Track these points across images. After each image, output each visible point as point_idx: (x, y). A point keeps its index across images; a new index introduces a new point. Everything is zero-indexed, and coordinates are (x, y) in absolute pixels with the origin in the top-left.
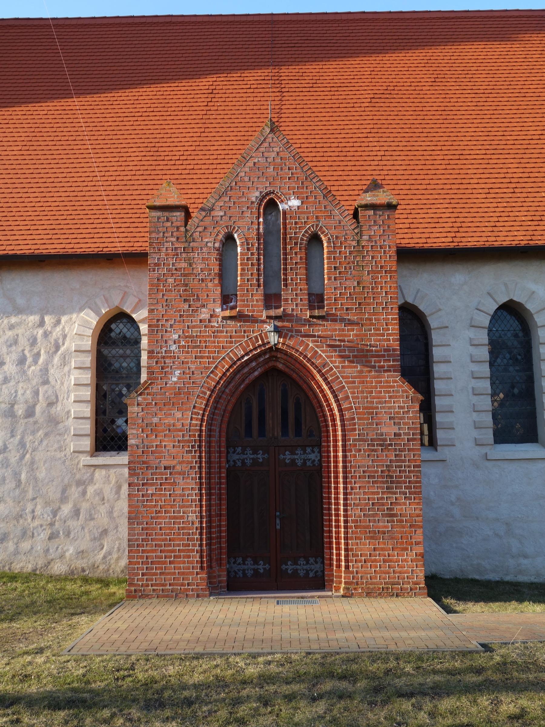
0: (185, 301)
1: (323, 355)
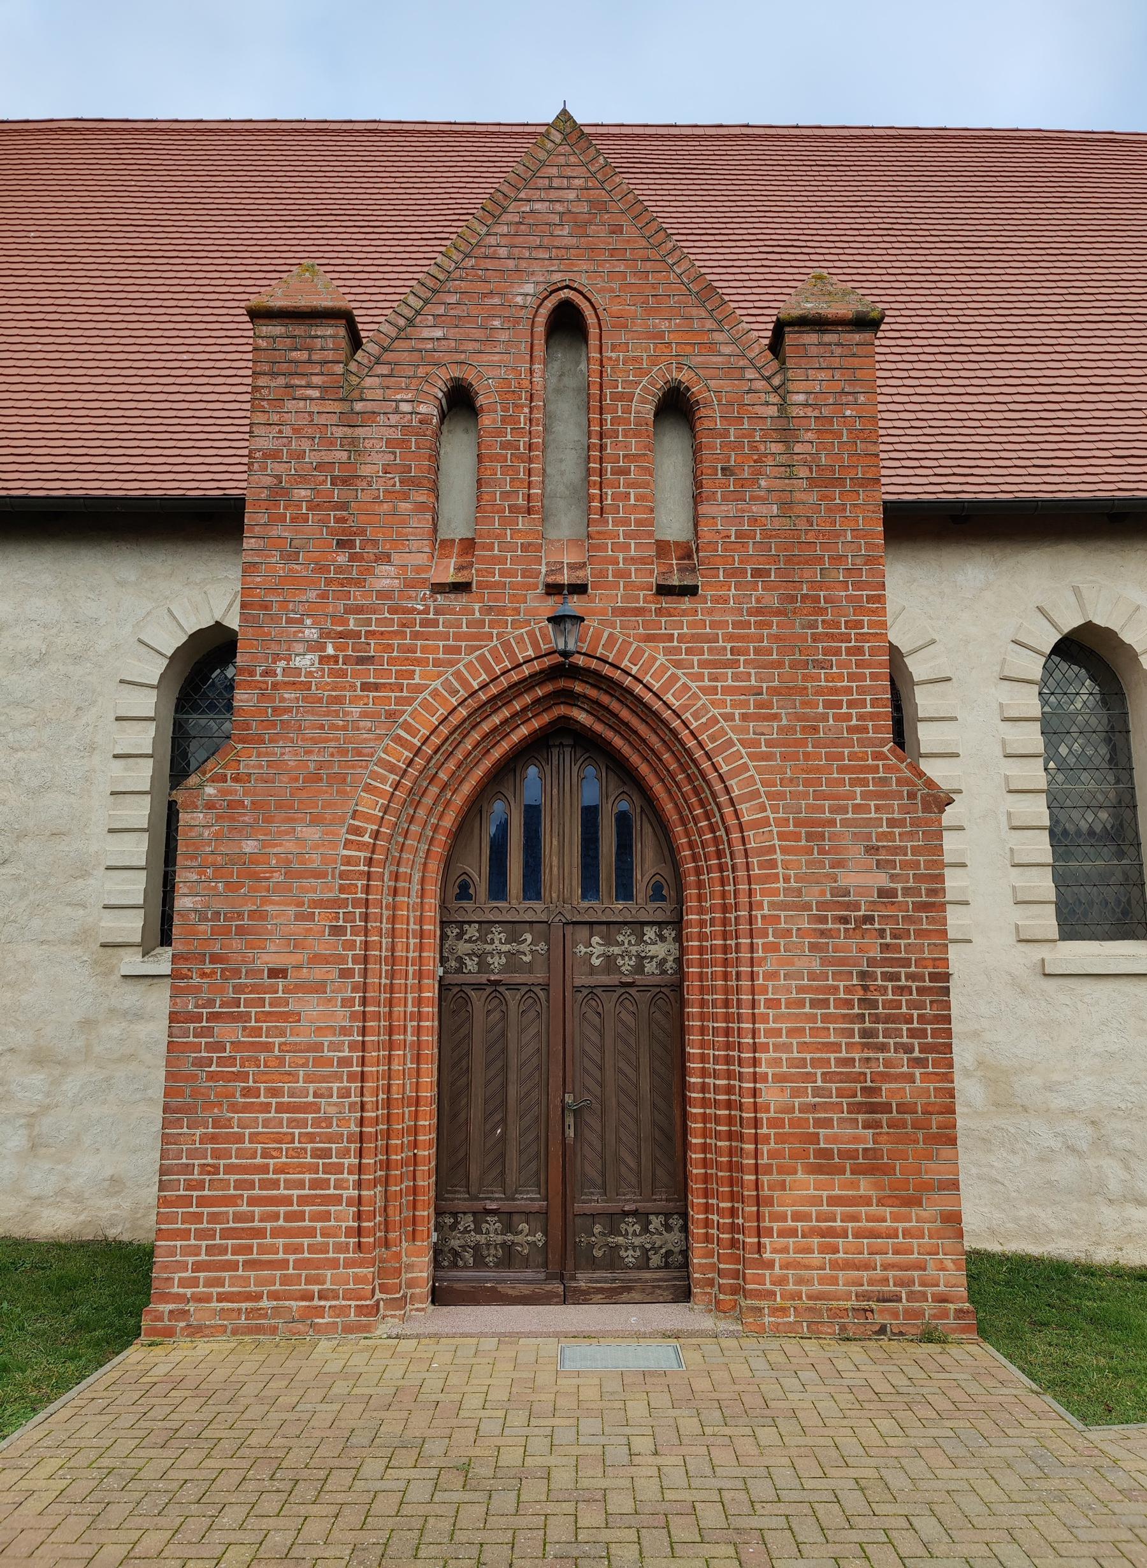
0: (341, 544)
1: (693, 685)
